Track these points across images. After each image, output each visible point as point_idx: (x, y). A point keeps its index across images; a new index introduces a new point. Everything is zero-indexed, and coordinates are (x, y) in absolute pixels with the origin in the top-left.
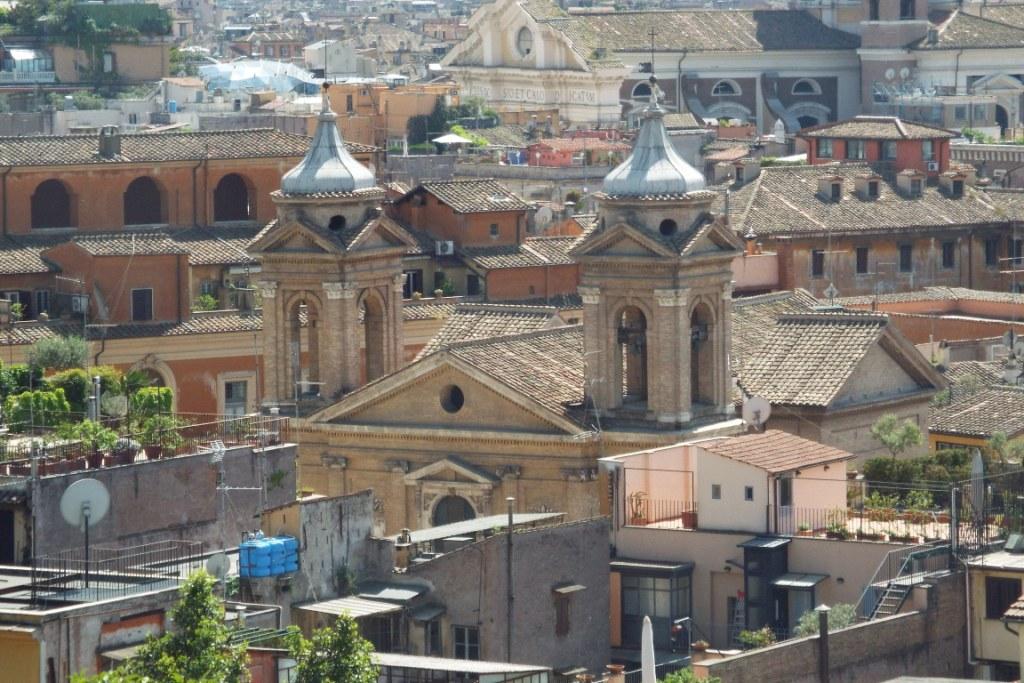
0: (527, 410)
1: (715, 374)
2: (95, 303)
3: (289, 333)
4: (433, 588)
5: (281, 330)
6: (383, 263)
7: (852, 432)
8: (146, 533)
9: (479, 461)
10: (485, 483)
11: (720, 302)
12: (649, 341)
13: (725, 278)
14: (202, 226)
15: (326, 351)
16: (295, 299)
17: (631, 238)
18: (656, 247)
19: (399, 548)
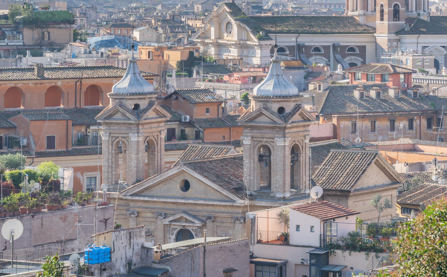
0: (218, 191)
1: (301, 176)
2: (30, 141)
3: (114, 155)
4: (170, 270)
5: (110, 154)
6: (156, 125)
7: (362, 202)
8: (46, 244)
9: (195, 213)
10: (198, 224)
11: (304, 144)
12: (272, 160)
13: (306, 133)
14: (79, 108)
15: (130, 164)
16: (117, 140)
17: (265, 115)
18: (275, 119)
19: (157, 252)
